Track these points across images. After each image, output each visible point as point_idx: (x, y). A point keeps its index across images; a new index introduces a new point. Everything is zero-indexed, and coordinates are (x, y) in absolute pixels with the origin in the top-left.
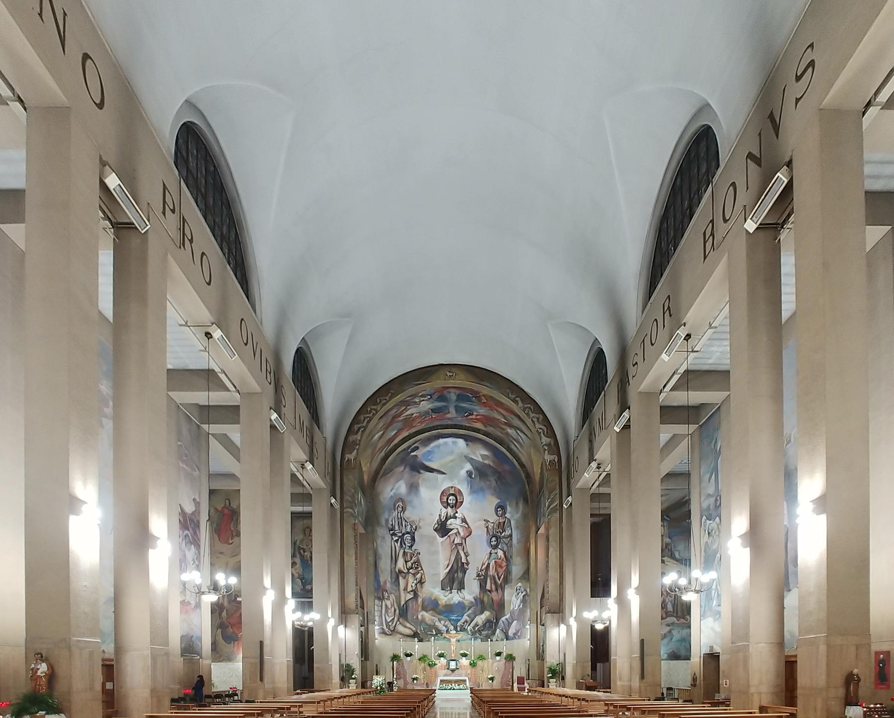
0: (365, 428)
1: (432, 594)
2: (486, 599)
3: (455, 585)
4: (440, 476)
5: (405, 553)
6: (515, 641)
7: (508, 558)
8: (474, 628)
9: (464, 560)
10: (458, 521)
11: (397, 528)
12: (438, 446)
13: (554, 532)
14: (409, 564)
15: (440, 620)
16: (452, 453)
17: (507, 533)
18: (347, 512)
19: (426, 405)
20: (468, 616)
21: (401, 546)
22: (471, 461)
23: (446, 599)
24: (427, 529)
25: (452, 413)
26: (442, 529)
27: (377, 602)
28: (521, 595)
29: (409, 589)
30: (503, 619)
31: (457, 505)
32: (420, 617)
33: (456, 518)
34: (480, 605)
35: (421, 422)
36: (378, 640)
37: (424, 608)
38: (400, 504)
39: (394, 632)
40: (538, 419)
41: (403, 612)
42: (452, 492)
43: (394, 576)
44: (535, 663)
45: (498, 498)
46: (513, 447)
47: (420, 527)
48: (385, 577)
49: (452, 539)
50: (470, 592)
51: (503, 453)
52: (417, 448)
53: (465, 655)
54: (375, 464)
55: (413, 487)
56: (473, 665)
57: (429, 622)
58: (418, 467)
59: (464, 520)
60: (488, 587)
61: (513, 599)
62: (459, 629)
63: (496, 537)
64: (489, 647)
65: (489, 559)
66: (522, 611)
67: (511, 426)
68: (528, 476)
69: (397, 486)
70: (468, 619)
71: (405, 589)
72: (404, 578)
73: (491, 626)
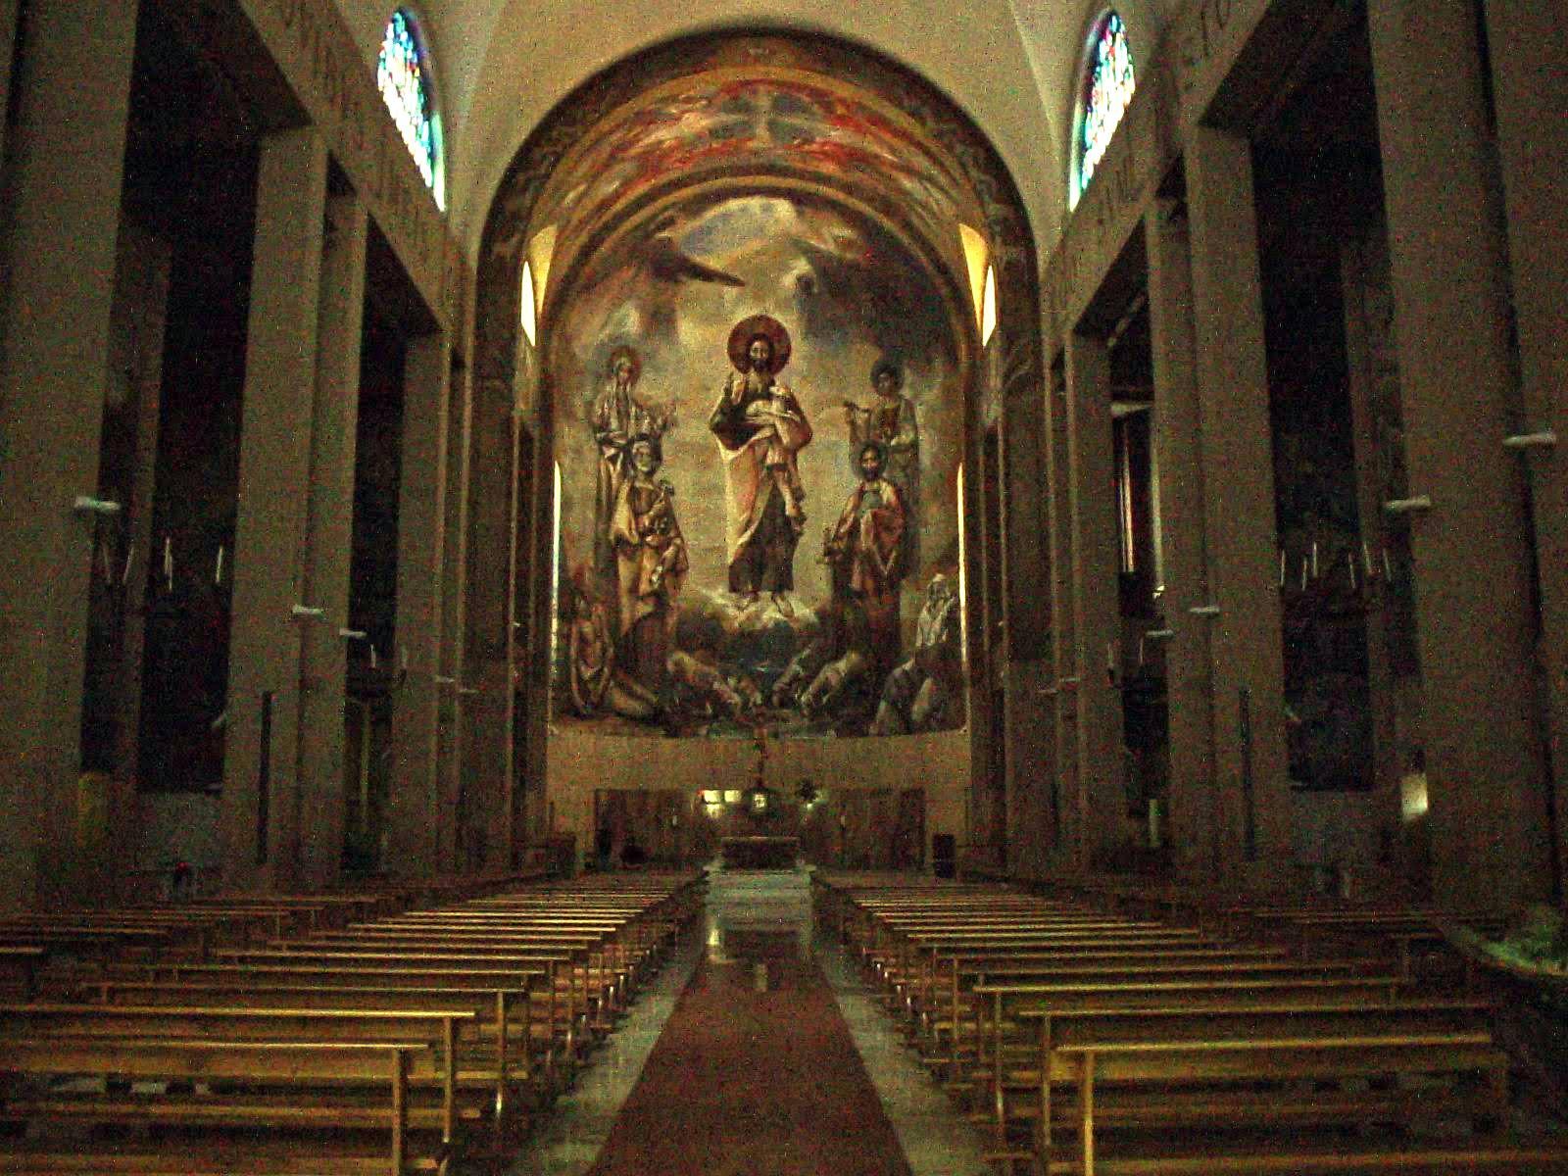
1: (707, 600)
2: (849, 617)
3: (768, 576)
4: (730, 292)
5: (634, 493)
8: (817, 696)
9: (789, 510)
10: (775, 406)
11: (614, 424)
15: (725, 676)
17: (906, 437)
21: (624, 474)
23: (742, 616)
29: (644, 587)
30: (897, 672)
31: (774, 363)
32: (670, 667)
33: (769, 397)
42: (760, 329)
43: (603, 550)
47: (675, 424)
52: (670, 223)
55: (660, 320)
58: (673, 269)
59: (790, 403)
65: (856, 507)
71: (634, 589)
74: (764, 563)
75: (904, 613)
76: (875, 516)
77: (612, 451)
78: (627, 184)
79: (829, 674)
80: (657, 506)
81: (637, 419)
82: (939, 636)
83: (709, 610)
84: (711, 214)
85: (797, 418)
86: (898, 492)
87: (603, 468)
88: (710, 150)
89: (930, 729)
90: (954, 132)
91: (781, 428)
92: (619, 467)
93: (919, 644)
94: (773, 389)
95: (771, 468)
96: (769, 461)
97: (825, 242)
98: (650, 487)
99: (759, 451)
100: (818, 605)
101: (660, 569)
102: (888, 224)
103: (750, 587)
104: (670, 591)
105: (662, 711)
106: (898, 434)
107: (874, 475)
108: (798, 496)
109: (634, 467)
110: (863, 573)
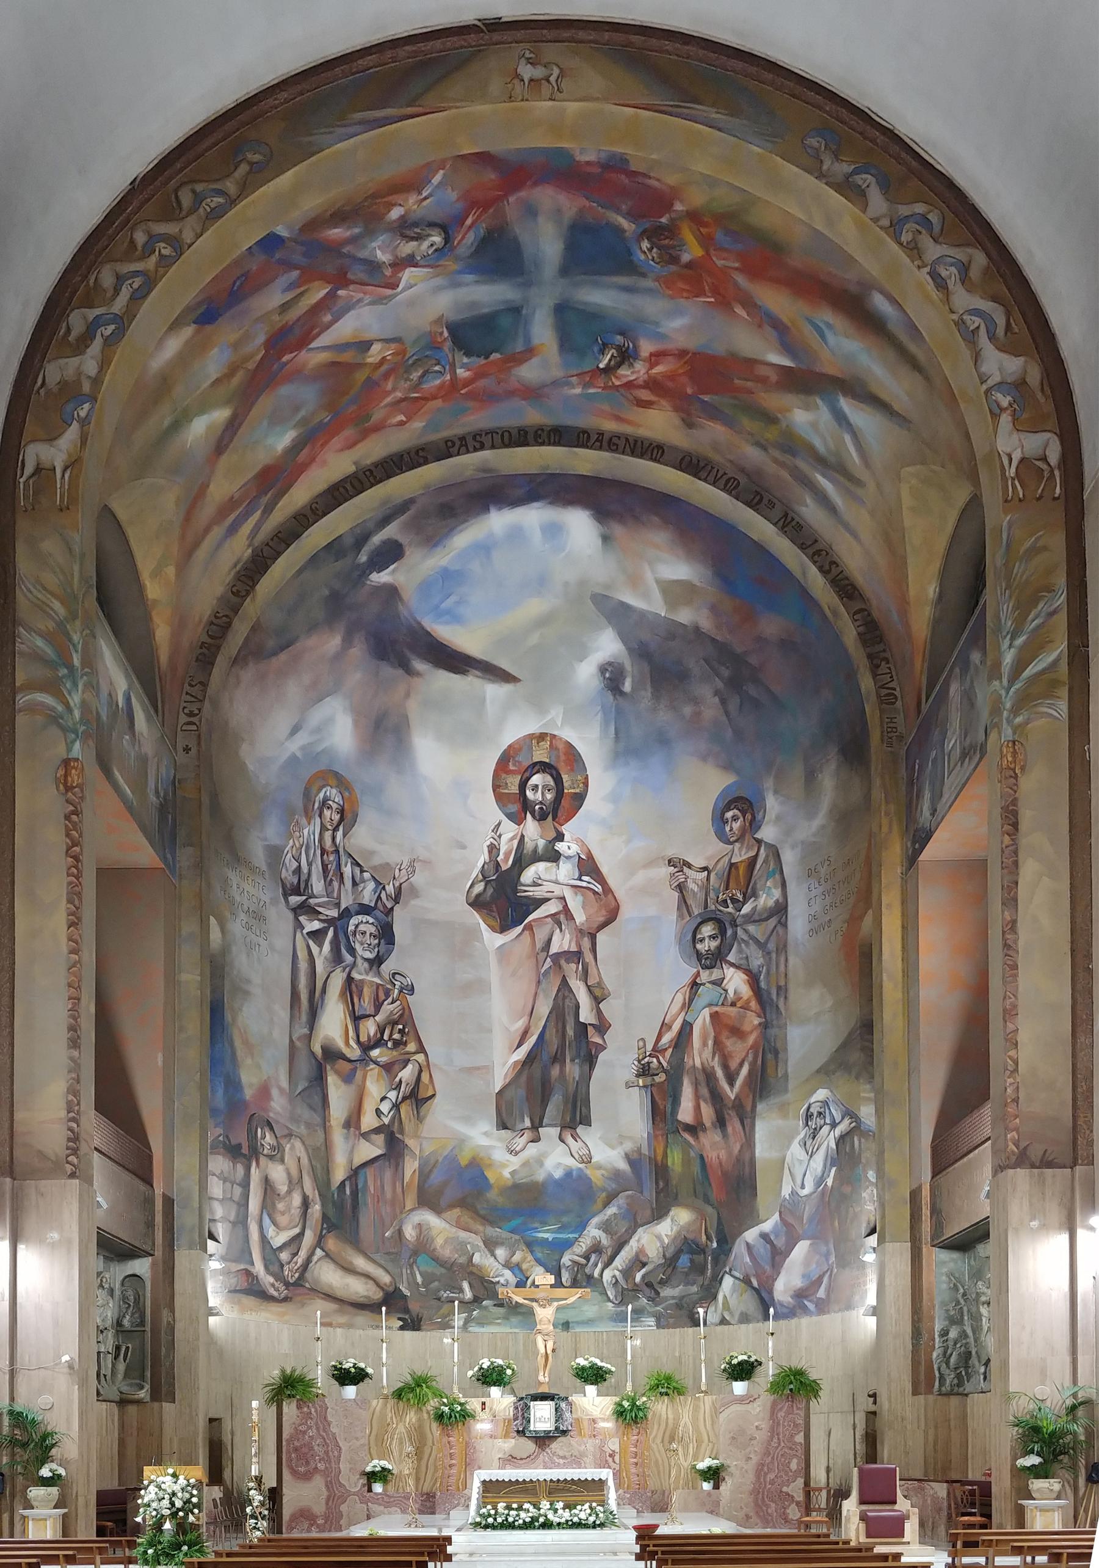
0: (123, 322)
1: (462, 1141)
2: (675, 1160)
3: (552, 1109)
4: (494, 691)
5: (350, 987)
6: (804, 1323)
7: (766, 997)
8: (628, 1273)
9: (586, 1015)
10: (565, 871)
11: (318, 885)
12: (484, 549)
13: (1042, 787)
14: (370, 1028)
15: (490, 1245)
16: (541, 583)
17: (766, 899)
18: (33, 709)
19: (426, 297)
20: (606, 1227)
21: (336, 958)
22: (618, 615)
23: (515, 1162)
24: (444, 897)
25: (544, 360)
26: (503, 898)
27: (219, 1163)
28: (828, 1139)
29: (369, 1121)
30: (751, 1235)
31: (562, 806)
32: (409, 1232)
33: (554, 857)
34: (654, 1183)
35: (411, 405)
36: (217, 1304)
37: (428, 1200)
38: (331, 796)
39: (297, 1289)
40: (964, 269)
41: (342, 1213)
42: (540, 755)
43: (305, 1068)
44: (906, 1411)
45: (727, 767)
46: (810, 511)
47: (414, 892)
48: (264, 1064)
49: (541, 935)
50: (614, 1133)
51: (760, 549)
52: (391, 553)
53: (594, 1376)
54: (209, 588)
55: (385, 732)
56: (630, 1416)
57: (446, 1253)
58: (406, 647)
59: (588, 866)
60: (685, 1113)
61: (792, 1157)
62: (566, 1277)
63: (720, 917)
64: (702, 1348)
65: (688, 1005)
66: (834, 1203)
67: (805, 381)
68: (872, 632)
69: (317, 715)
70: (605, 1241)
71: (352, 1122)
72: (348, 1079)
73: (698, 1264)
74: (549, 1083)
75: (762, 1150)
76: (714, 1016)
77: (316, 925)
78: (312, 439)
79: (643, 1241)
80: (387, 1008)
81: (355, 884)
82: (820, 1181)
83: (464, 1159)
84: (465, 537)
85: (598, 888)
86: (754, 980)
87: (302, 955)
88: (455, 385)
89: (805, 1310)
90: (924, 221)
91: (575, 903)
92: (327, 947)
93: (786, 1191)
94: (560, 846)
95: (556, 957)
96: (554, 949)
97: (646, 596)
98: (377, 980)
99: (541, 935)
100: (628, 1146)
101: (392, 1095)
102: (760, 528)
103: (527, 1123)
104: (408, 1126)
105: (397, 1290)
106: (755, 895)
107: (714, 959)
108: (598, 998)
109: (352, 951)
110: (697, 1097)
